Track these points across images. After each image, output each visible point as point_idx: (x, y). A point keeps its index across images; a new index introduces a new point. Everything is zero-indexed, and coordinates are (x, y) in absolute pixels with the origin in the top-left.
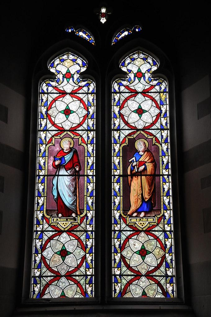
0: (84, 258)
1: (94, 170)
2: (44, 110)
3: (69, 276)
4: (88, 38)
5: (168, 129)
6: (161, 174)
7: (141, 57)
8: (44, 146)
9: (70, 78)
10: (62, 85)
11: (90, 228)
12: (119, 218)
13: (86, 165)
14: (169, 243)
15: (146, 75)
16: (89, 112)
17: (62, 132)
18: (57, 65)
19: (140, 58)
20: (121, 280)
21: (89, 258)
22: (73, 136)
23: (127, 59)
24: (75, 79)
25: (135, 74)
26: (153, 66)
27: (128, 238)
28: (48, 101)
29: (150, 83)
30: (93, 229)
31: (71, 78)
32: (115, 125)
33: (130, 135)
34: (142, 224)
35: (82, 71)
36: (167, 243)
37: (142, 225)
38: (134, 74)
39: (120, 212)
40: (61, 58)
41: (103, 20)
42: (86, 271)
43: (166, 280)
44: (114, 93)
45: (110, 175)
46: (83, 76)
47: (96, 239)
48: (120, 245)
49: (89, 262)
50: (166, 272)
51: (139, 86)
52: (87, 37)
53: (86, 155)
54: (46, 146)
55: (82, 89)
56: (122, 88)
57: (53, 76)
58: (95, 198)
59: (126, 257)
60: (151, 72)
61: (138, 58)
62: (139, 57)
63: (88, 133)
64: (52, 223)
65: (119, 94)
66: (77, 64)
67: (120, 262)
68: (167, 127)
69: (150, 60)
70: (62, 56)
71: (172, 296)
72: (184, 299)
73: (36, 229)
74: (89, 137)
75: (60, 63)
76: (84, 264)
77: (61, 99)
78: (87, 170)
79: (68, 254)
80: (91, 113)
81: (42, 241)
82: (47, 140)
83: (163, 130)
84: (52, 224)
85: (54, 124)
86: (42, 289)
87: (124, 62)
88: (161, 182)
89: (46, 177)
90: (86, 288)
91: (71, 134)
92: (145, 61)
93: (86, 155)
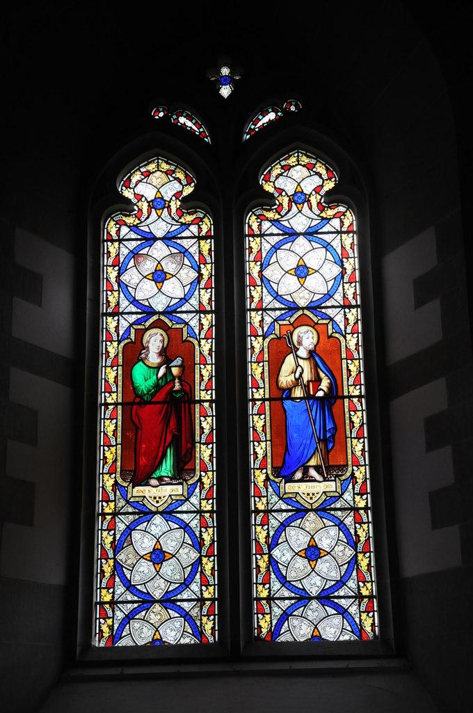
0: (354, 562)
1: (214, 391)
2: (113, 274)
3: (325, 598)
4: (196, 129)
5: (248, 310)
6: (346, 394)
7: (303, 163)
8: (115, 344)
9: (303, 203)
10: (149, 221)
11: (207, 506)
12: (112, 490)
13: (345, 377)
14: (364, 532)
15: (172, 204)
16: (345, 269)
17: (293, 312)
18: (277, 177)
19: (161, 171)
20: (270, 607)
21: (208, 565)
22: (315, 319)
23: (274, 166)
24: (174, 210)
25: (291, 197)
26: (327, 180)
27: (284, 526)
28: (263, 251)
29: (180, 220)
30: (213, 507)
31: (306, 204)
32: (108, 306)
33: (137, 322)
34: (311, 495)
35: (185, 194)
36: (360, 532)
37: (157, 502)
38: (148, 202)
39: (115, 477)
40: (283, 163)
41: (225, 91)
42: (201, 590)
43: (359, 605)
44: (249, 236)
45: (244, 400)
46: (188, 204)
47: (375, 523)
48: (268, 537)
49: (208, 572)
50: (359, 590)
51: (300, 222)
52: (194, 127)
53: (344, 355)
54: (118, 344)
55: (187, 228)
56: (125, 230)
57: (129, 207)
58: (216, 446)
59: (279, 561)
60: (322, 192)
61: (156, 171)
62: (298, 161)
63: (345, 312)
64: (285, 493)
65: (117, 243)
66: (176, 179)
67: (113, 576)
68: (356, 301)
69: (181, 175)
70: (146, 165)
71: (211, 640)
72: (394, 647)
73: (102, 511)
74: (202, 325)
75: (143, 179)
76: (198, 576)
77: (287, 246)
78: (348, 385)
79: (321, 555)
80: (349, 272)
81: (114, 534)
82: (121, 333)
83: (204, 314)
84: (285, 496)
85: (134, 302)
86: (274, 624)
87: (129, 180)
88: (197, 415)
89: (120, 407)
90: (360, 620)
91: (311, 316)
92: (312, 170)
93: (344, 355)
